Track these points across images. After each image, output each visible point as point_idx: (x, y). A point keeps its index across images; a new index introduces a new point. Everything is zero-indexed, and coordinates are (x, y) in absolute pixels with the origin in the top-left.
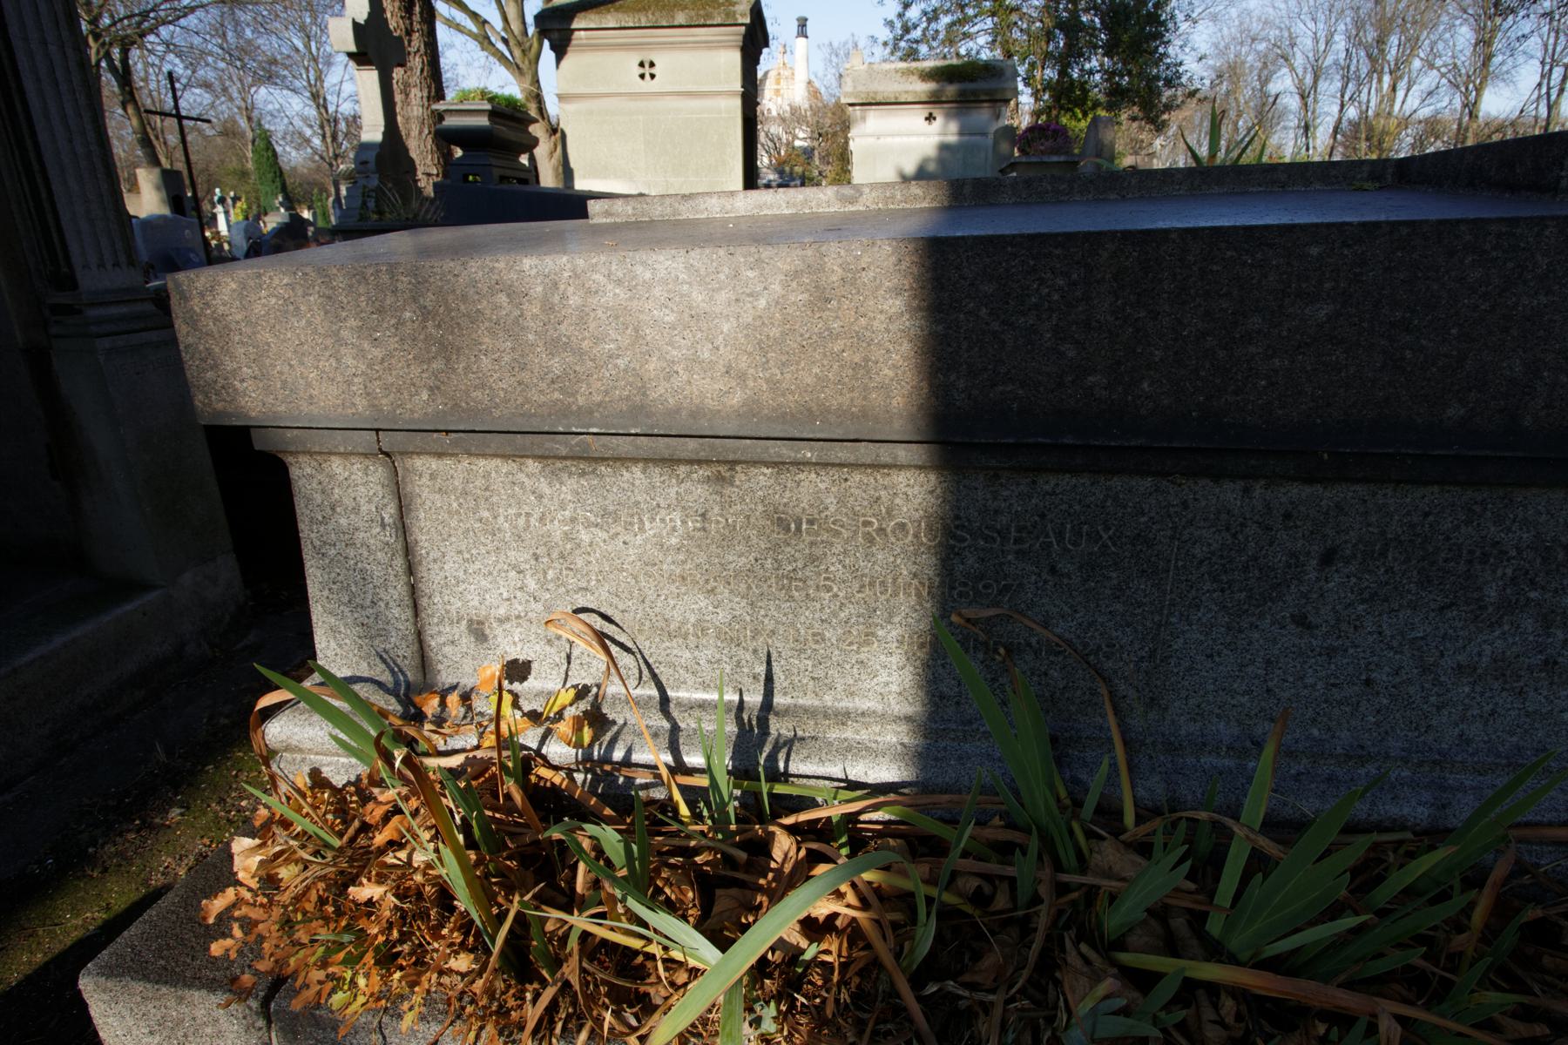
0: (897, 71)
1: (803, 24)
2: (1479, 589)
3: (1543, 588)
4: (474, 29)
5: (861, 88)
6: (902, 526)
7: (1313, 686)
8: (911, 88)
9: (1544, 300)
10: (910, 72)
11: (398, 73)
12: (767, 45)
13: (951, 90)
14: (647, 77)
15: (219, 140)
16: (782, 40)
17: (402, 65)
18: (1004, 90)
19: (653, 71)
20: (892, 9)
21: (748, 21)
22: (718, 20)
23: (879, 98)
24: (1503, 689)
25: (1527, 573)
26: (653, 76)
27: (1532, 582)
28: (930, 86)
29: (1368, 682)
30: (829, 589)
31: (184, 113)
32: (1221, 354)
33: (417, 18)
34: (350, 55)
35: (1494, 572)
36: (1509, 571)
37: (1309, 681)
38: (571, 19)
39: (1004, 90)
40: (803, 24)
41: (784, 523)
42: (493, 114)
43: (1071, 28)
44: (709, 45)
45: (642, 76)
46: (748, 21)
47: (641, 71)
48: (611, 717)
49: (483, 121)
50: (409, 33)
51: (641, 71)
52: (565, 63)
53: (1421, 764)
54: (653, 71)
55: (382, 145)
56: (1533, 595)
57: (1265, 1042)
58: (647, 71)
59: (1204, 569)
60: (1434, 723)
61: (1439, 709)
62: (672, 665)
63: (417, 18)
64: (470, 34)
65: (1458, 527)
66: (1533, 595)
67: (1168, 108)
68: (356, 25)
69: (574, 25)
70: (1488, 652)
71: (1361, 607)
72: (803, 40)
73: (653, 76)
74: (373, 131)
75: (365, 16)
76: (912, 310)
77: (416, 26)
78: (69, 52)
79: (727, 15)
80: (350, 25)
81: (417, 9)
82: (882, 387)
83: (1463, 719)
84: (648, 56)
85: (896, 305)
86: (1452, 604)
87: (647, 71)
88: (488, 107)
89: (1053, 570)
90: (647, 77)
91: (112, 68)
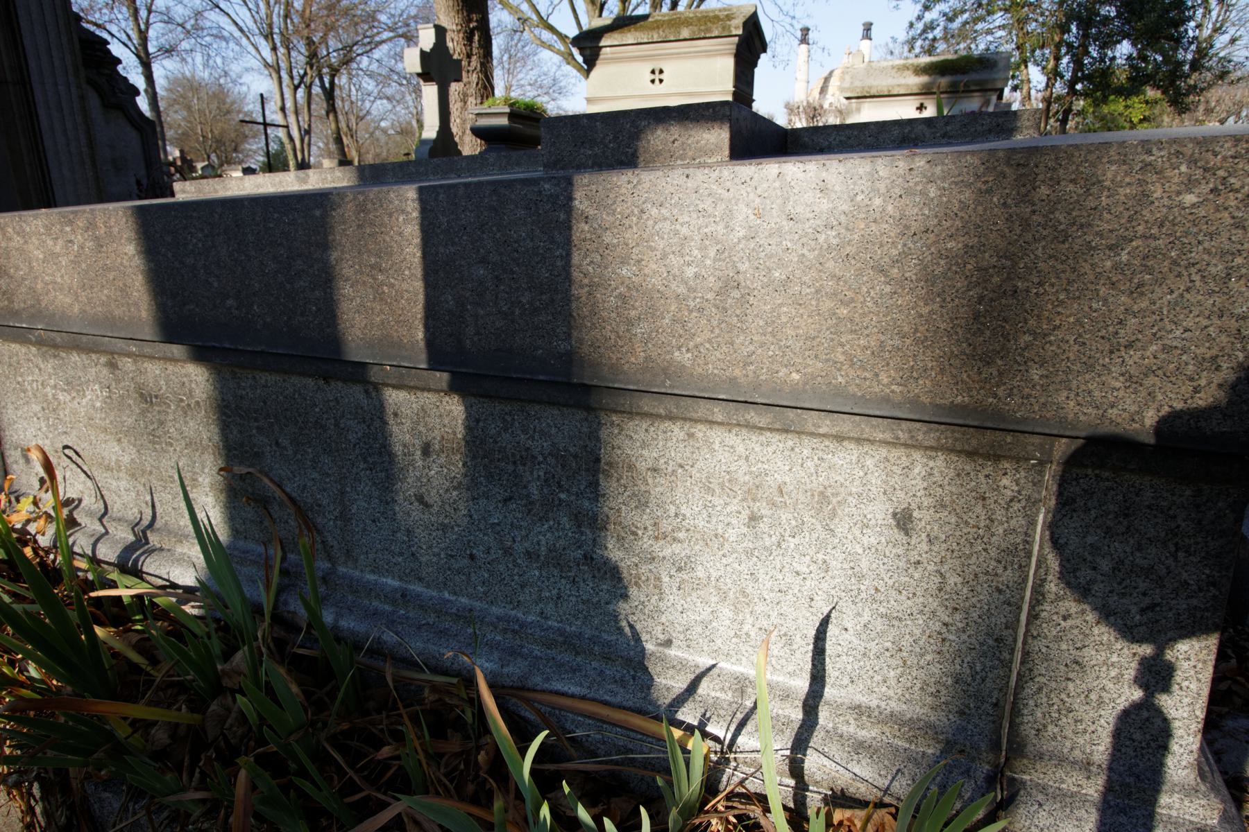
0: (893, 67)
1: (868, 28)
2: (525, 487)
3: (568, 491)
4: (562, 49)
5: (858, 83)
6: (198, 403)
7: (439, 554)
8: (903, 81)
9: (452, 250)
10: (906, 68)
11: (455, 88)
12: (765, 51)
13: (944, 81)
14: (657, 82)
15: (398, 138)
16: (821, 44)
17: (459, 80)
18: (994, 80)
19: (662, 77)
20: (911, 10)
21: (740, 32)
22: (716, 33)
23: (873, 92)
24: (562, 577)
25: (553, 476)
26: (661, 81)
27: (560, 486)
28: (924, 79)
29: (472, 557)
30: (171, 445)
31: (268, 120)
32: (288, 286)
33: (475, 45)
34: (419, 75)
35: (532, 473)
36: (541, 474)
37: (436, 550)
38: (600, 39)
39: (994, 80)
40: (868, 28)
41: (147, 398)
42: (513, 116)
43: (1087, 20)
44: (708, 54)
45: (653, 81)
46: (740, 32)
47: (652, 77)
48: (79, 520)
49: (504, 121)
50: (469, 56)
51: (652, 77)
52: (593, 74)
53: (505, 631)
54: (662, 77)
55: (435, 141)
56: (563, 496)
57: (338, 829)
58: (657, 77)
59: (357, 451)
60: (521, 598)
61: (522, 587)
62: (109, 490)
63: (475, 45)
64: (558, 52)
65: (499, 433)
66: (563, 496)
67: (1193, 89)
68: (423, 53)
69: (602, 44)
70: (543, 542)
71: (455, 493)
72: (867, 41)
73: (661, 81)
74: (431, 131)
75: (431, 46)
76: (139, 253)
77: (475, 51)
78: (73, 90)
79: (724, 28)
80: (418, 53)
81: (476, 38)
82: (136, 304)
83: (540, 599)
84: (657, 65)
85: (131, 249)
86: (511, 498)
87: (657, 77)
88: (507, 110)
89: (277, 444)
90: (657, 82)
91: (323, 86)
